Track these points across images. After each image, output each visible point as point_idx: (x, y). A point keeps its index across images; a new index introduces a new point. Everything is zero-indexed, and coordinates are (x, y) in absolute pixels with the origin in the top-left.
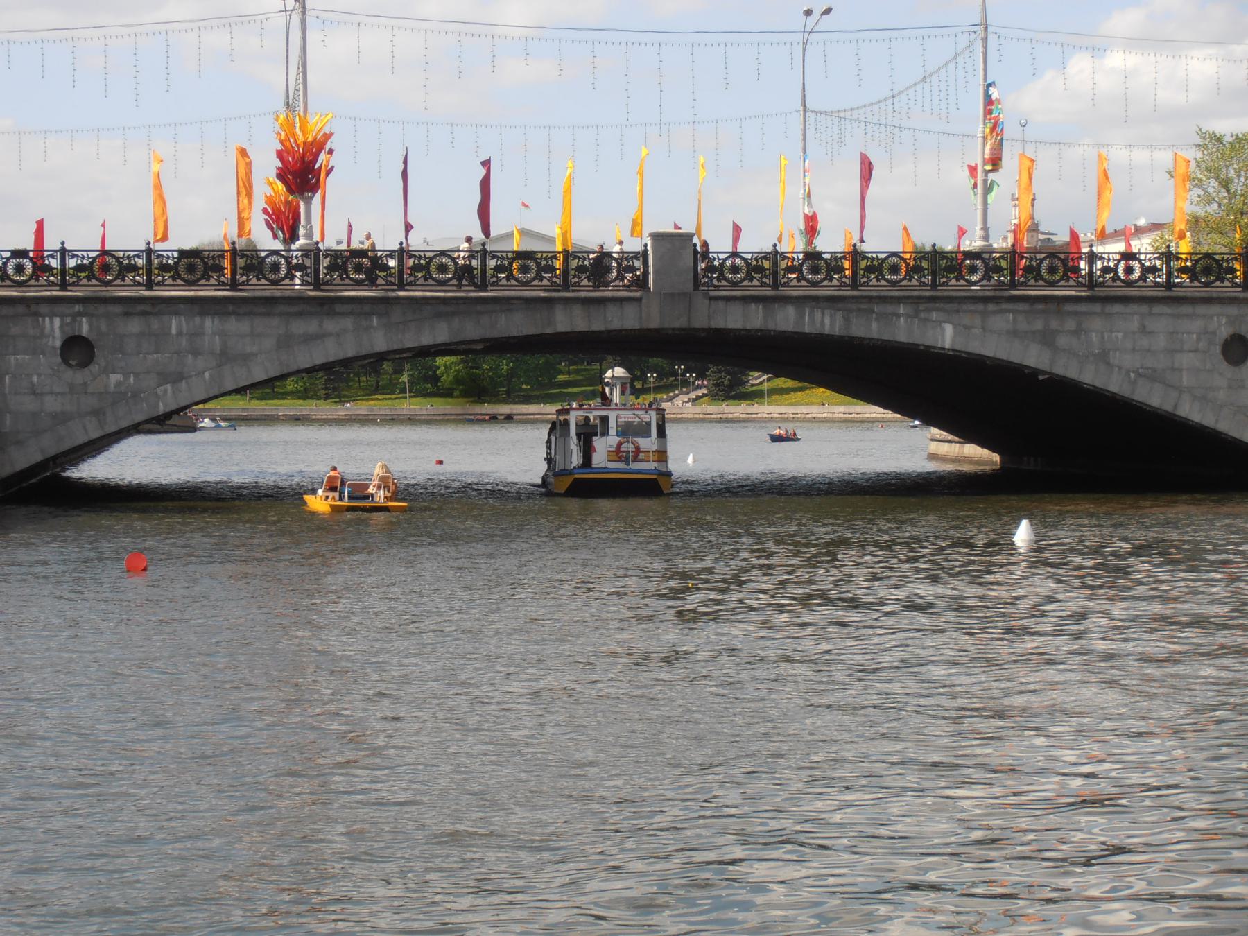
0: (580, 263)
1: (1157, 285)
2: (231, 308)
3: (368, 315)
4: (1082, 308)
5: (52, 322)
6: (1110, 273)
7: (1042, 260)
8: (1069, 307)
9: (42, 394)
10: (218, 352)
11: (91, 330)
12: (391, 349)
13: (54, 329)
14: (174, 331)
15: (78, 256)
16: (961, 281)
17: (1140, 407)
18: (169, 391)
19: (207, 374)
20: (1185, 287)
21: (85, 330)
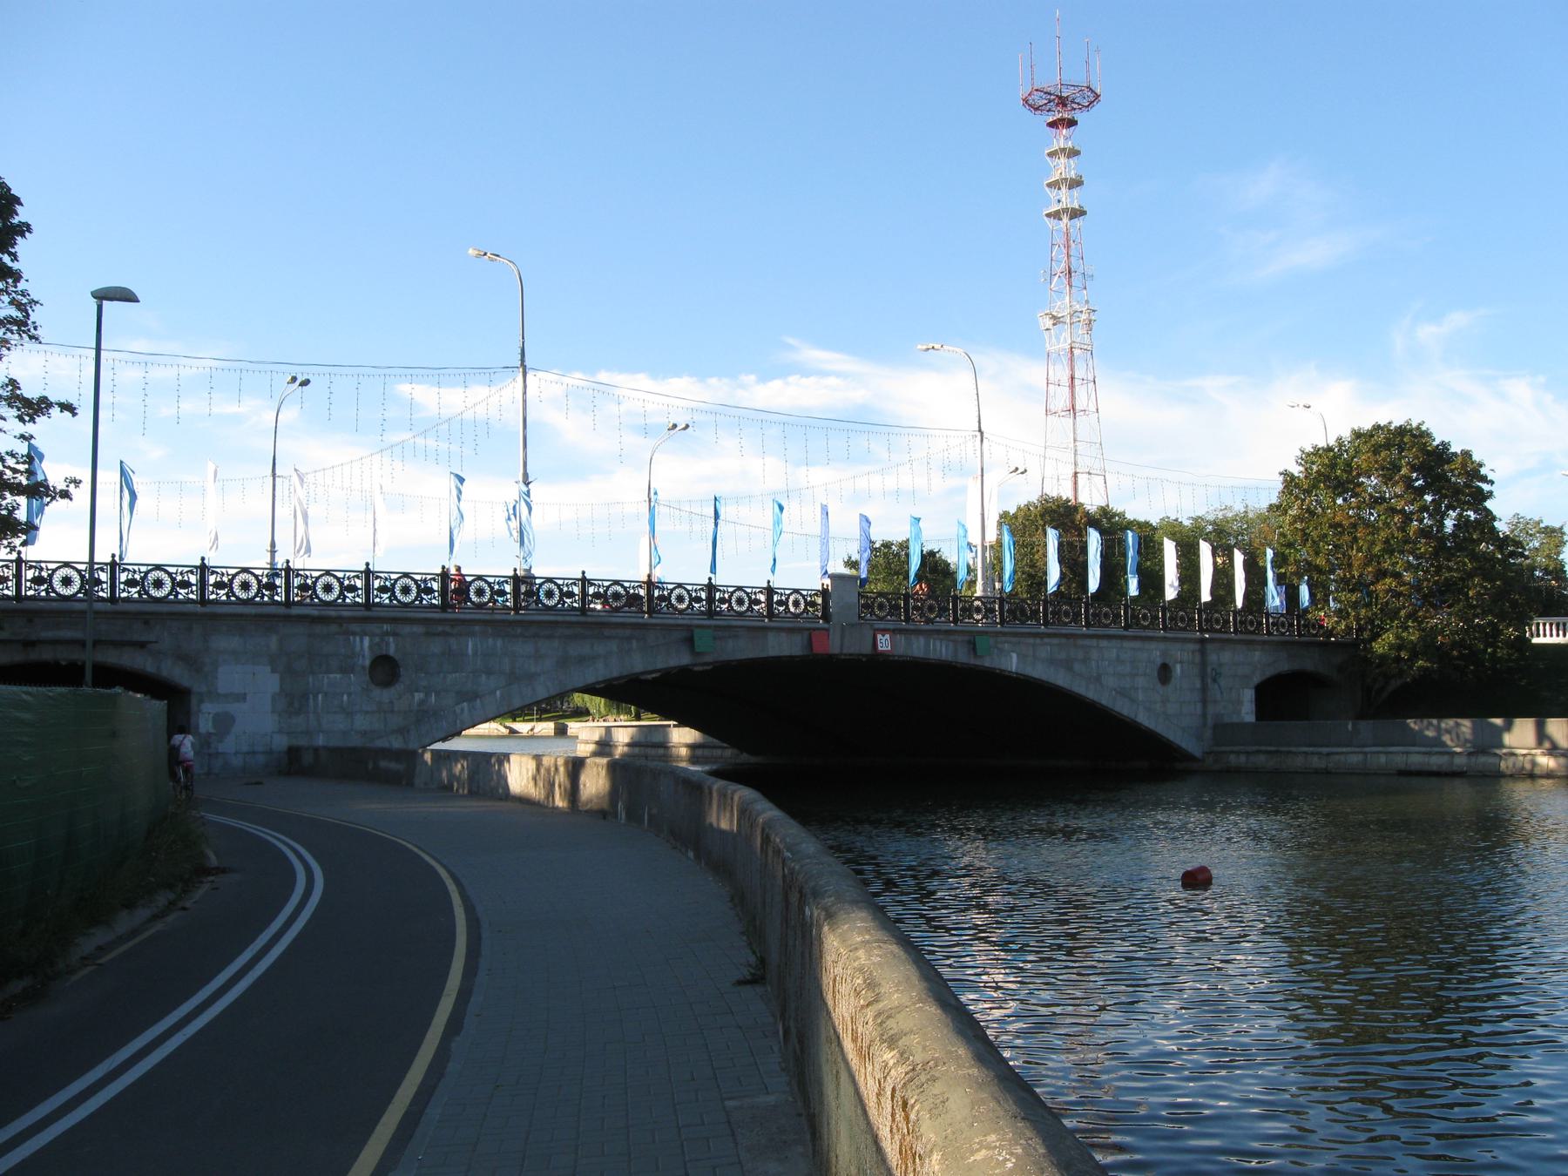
0: (218, 579)
1: (356, 604)
2: (519, 631)
4: (1087, 642)
5: (362, 641)
6: (224, 589)
8: (1080, 642)
15: (129, 570)
18: (466, 709)
21: (392, 651)
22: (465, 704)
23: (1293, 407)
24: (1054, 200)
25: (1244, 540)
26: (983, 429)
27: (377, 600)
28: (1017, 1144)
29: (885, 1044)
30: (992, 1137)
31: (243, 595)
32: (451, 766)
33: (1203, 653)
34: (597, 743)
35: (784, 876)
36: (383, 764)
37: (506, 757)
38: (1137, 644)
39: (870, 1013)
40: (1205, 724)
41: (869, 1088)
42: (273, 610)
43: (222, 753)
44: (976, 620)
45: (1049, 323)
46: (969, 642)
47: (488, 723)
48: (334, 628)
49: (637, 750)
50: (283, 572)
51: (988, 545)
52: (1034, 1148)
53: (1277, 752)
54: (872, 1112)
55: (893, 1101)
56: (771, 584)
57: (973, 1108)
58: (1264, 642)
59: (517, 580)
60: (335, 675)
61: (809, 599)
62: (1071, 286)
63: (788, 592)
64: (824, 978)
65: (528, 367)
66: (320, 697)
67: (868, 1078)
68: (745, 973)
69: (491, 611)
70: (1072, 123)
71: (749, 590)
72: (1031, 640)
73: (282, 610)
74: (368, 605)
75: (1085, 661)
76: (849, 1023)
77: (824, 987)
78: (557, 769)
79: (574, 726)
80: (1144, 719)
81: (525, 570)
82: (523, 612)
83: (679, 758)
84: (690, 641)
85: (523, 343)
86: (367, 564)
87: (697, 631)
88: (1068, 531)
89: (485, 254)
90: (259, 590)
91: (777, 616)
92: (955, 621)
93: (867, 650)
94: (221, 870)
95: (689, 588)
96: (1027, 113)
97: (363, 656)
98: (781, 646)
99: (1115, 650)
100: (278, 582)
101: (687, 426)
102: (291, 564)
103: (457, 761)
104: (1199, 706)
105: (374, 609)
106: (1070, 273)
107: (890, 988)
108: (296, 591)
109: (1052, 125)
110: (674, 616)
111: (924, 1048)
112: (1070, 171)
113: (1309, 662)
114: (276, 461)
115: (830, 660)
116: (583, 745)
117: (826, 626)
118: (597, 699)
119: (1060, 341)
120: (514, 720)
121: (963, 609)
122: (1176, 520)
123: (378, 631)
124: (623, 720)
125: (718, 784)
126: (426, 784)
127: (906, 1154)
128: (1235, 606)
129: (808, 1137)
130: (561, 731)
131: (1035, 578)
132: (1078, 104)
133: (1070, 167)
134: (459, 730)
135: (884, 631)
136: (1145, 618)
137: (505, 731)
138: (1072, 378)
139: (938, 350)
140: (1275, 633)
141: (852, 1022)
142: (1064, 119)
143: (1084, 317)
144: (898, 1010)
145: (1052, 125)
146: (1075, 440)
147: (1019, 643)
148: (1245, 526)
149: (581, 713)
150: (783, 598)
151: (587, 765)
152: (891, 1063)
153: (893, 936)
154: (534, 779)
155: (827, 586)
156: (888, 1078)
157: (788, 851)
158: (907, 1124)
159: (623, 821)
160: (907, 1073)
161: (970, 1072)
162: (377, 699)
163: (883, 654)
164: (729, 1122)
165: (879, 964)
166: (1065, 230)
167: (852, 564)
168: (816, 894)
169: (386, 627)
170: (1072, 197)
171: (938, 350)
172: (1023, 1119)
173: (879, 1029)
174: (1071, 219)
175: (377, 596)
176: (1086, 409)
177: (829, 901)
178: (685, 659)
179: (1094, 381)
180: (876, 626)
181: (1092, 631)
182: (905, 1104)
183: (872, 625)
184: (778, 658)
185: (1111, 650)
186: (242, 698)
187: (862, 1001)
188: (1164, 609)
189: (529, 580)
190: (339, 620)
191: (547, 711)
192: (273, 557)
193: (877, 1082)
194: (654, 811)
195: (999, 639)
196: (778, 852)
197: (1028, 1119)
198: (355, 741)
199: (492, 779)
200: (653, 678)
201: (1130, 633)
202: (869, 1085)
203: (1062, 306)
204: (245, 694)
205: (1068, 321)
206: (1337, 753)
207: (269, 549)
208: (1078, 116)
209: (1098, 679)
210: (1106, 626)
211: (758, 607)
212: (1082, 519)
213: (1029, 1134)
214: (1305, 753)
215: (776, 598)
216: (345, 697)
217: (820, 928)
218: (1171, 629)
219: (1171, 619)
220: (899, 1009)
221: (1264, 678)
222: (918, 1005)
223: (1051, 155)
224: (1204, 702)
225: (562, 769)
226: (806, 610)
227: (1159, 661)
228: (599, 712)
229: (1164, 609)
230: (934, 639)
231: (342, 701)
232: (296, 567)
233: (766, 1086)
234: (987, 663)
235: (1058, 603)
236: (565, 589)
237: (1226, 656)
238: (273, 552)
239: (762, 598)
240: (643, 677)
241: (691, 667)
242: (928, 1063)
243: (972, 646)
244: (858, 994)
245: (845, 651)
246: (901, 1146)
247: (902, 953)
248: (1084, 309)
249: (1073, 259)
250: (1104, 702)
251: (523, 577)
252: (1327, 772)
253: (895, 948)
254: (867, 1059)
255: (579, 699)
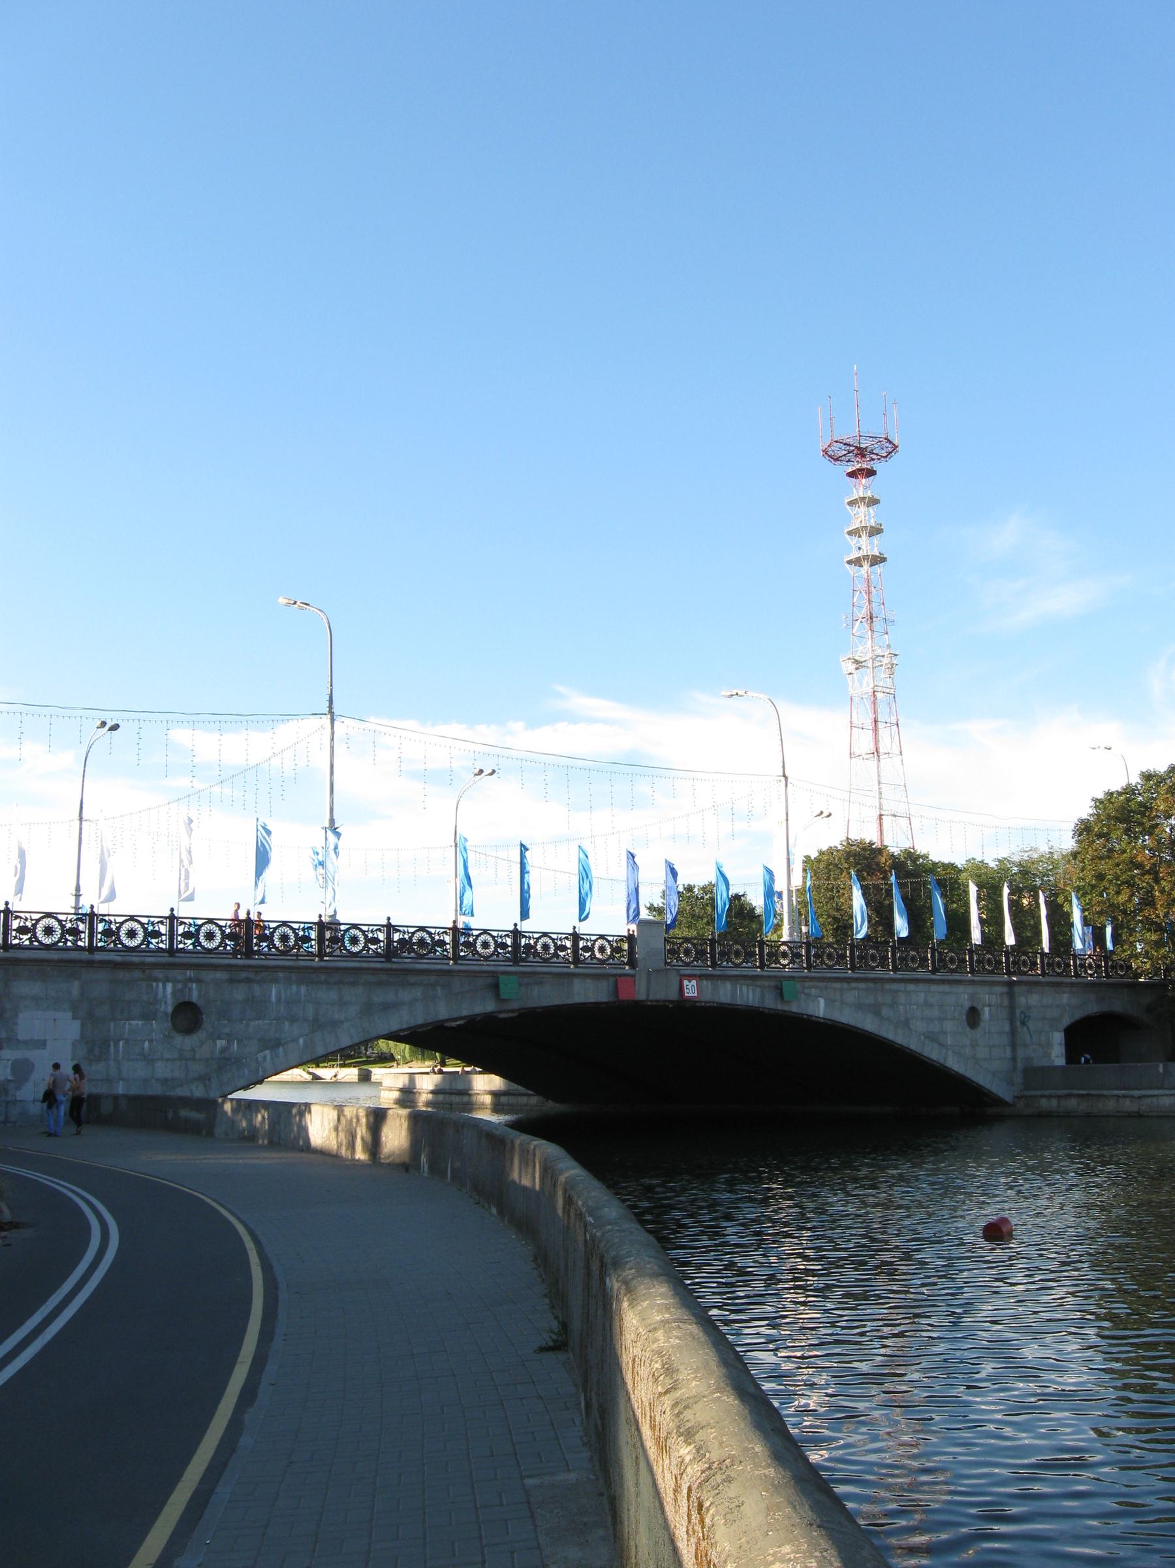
0: (22, 924)
1: (377, 955)
2: (323, 977)
3: (434, 986)
4: (895, 986)
5: (165, 988)
6: (26, 934)
7: (478, 936)
8: (888, 986)
9: (153, 1060)
10: (311, 1019)
11: (199, 996)
12: (452, 1017)
13: (167, 993)
14: (273, 999)
16: (537, 958)
17: (925, 1061)
18: (268, 1058)
19: (301, 1040)
20: (468, 960)
21: (194, 997)
22: (267, 1052)
23: (1094, 748)
24: (854, 548)
25: (1050, 881)
26: (787, 774)
27: (181, 946)
28: (812, 1556)
29: (682, 1438)
30: (787, 1549)
31: (47, 941)
32: (251, 1115)
33: (1011, 995)
34: (401, 1090)
35: (585, 1240)
36: (184, 1113)
37: (307, 1106)
38: (946, 988)
39: (668, 1401)
40: (1015, 1068)
41: (666, 1483)
42: (74, 955)
43: (21, 1101)
44: (782, 965)
45: (851, 667)
46: (776, 988)
47: (291, 1070)
48: (137, 974)
49: (441, 1098)
50: (88, 917)
51: (794, 889)
52: (829, 1561)
53: (1089, 1095)
54: (669, 1509)
55: (688, 1500)
56: (577, 930)
57: (768, 1515)
58: (1072, 984)
59: (321, 926)
60: (137, 1022)
61: (615, 944)
62: (872, 631)
63: (593, 938)
64: (624, 1357)
65: (336, 714)
66: (121, 1043)
67: (666, 1472)
68: (547, 1339)
69: (295, 958)
70: (871, 473)
71: (554, 936)
72: (838, 985)
73: (85, 956)
74: (172, 951)
75: (893, 1005)
76: (648, 1409)
77: (624, 1365)
78: (358, 1120)
79: (377, 1072)
80: (954, 1064)
81: (330, 916)
82: (328, 958)
83: (482, 1107)
84: (495, 987)
85: (331, 690)
86: (172, 910)
87: (502, 978)
88: (873, 874)
89: (295, 603)
90: (62, 936)
91: (583, 962)
92: (762, 966)
93: (673, 995)
94: (14, 1225)
95: (495, 934)
96: (826, 461)
97: (166, 1003)
98: (586, 993)
99: (923, 995)
100: (81, 927)
101: (494, 772)
102: (95, 910)
103: (258, 1111)
104: (1008, 1050)
105: (177, 955)
106: (871, 618)
107: (689, 1374)
108: (99, 936)
109: (852, 475)
110: (479, 963)
111: (721, 1443)
112: (869, 521)
113: (1118, 1004)
114: (84, 805)
115: (638, 1007)
116: (387, 1092)
117: (632, 972)
118: (402, 1046)
119: (863, 684)
120: (318, 1066)
121: (769, 954)
122: (982, 862)
123: (180, 977)
124: (426, 1067)
125: (521, 1138)
126: (226, 1134)
127: (701, 1560)
128: (1042, 949)
129: (610, 1519)
130: (365, 1077)
131: (843, 925)
132: (877, 455)
133: (869, 515)
134: (260, 1078)
135: (690, 977)
136: (952, 960)
137: (309, 1078)
138: (876, 721)
139: (742, 696)
140: (1083, 975)
141: (650, 1409)
142: (863, 469)
143: (886, 661)
144: (696, 1400)
145: (852, 475)
146: (879, 783)
147: (826, 988)
148: (1051, 867)
149: (386, 1059)
150: (589, 944)
151: (389, 1117)
152: (687, 1459)
153: (694, 1315)
154: (336, 1129)
155: (633, 931)
156: (684, 1476)
157: (590, 1216)
158: (703, 1528)
159: (426, 1175)
160: (703, 1472)
161: (766, 1472)
162: (179, 1047)
163: (690, 999)
164: (529, 1503)
165: (679, 1346)
166: (866, 577)
167: (659, 911)
168: (617, 1264)
169: (190, 973)
170: (872, 544)
171: (742, 696)
172: (819, 1526)
173: (676, 1420)
174: (871, 565)
175: (181, 942)
176: (890, 752)
177: (629, 1273)
178: (488, 1006)
179: (897, 725)
180: (682, 972)
181: (900, 975)
182: (700, 1506)
183: (678, 971)
184: (583, 1006)
185: (919, 994)
186: (42, 1044)
187: (660, 1388)
188: (971, 952)
189: (334, 927)
190: (141, 966)
191: (350, 1057)
192: (77, 901)
193: (674, 1477)
194: (458, 1165)
195: (807, 984)
196: (580, 1216)
197: (824, 1528)
198: (156, 1090)
199: (292, 1131)
200: (458, 1025)
201: (937, 976)
202: (666, 1479)
203: (864, 650)
204: (45, 1041)
205: (870, 665)
206: (1149, 1096)
207: (74, 893)
208: (876, 466)
209: (906, 1024)
210: (914, 970)
211: (564, 953)
212: (886, 861)
213: (824, 1543)
214: (1118, 1096)
215: (581, 944)
216: (147, 1044)
217: (620, 1302)
218: (978, 972)
219: (978, 962)
220: (697, 1398)
221: (1073, 1020)
222: (715, 1395)
223: (851, 503)
224: (1013, 1046)
225: (364, 1120)
226: (612, 957)
227: (967, 1005)
228: (404, 1057)
229: (971, 952)
230: (741, 985)
231: (143, 1048)
232: (100, 913)
233: (567, 1462)
234: (794, 1008)
235: (865, 947)
236: (370, 935)
237: (1034, 999)
238: (78, 896)
239: (568, 944)
240: (447, 1025)
241: (496, 1015)
242: (724, 1461)
243: (778, 991)
244: (656, 1380)
245: (651, 997)
246: (697, 1549)
247: (701, 1334)
248: (886, 654)
249: (874, 605)
250: (913, 1047)
251: (327, 923)
252: (1139, 1115)
253: (694, 1329)
254: (664, 1452)
255: (383, 1045)
